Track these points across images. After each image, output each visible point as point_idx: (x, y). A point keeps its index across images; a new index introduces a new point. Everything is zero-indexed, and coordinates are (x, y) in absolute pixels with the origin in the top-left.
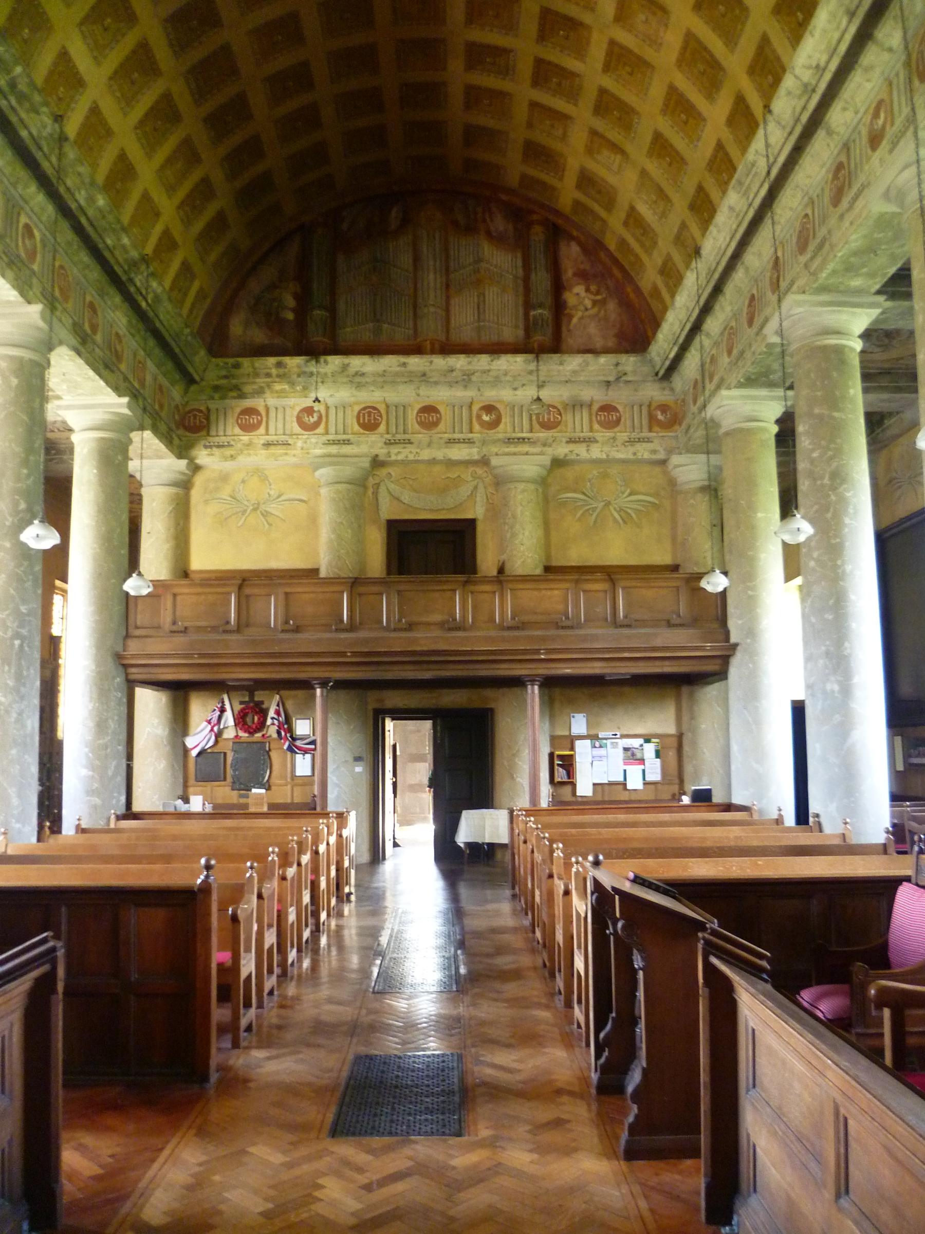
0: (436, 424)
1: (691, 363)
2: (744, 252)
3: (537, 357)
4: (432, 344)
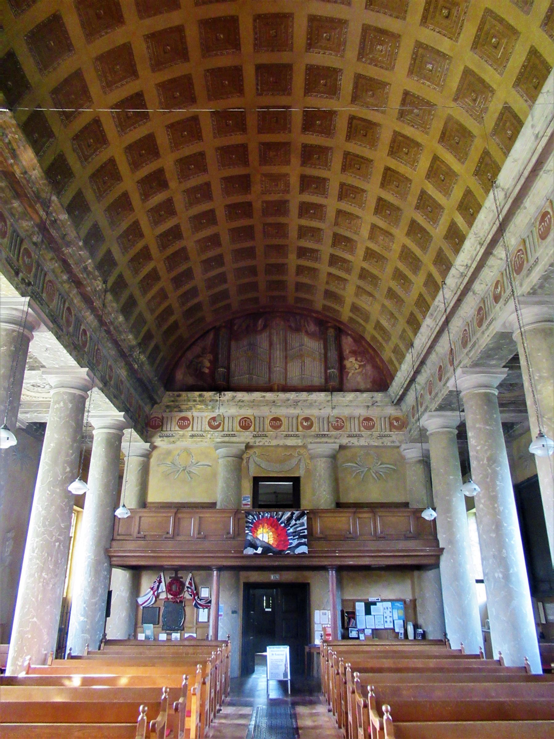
0: (279, 427)
1: (410, 398)
2: (435, 345)
3: (332, 394)
4: (278, 386)
